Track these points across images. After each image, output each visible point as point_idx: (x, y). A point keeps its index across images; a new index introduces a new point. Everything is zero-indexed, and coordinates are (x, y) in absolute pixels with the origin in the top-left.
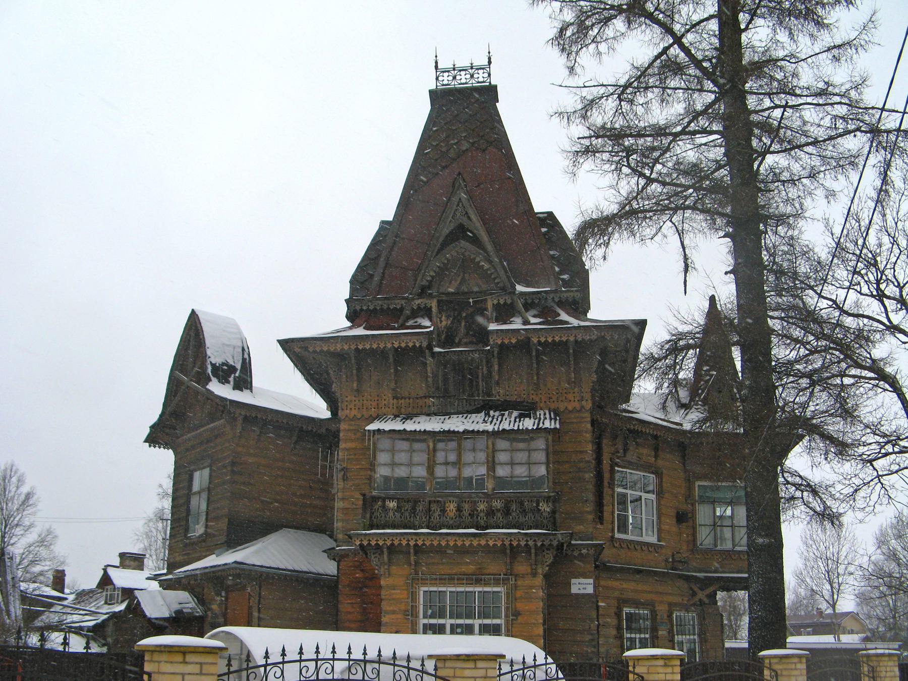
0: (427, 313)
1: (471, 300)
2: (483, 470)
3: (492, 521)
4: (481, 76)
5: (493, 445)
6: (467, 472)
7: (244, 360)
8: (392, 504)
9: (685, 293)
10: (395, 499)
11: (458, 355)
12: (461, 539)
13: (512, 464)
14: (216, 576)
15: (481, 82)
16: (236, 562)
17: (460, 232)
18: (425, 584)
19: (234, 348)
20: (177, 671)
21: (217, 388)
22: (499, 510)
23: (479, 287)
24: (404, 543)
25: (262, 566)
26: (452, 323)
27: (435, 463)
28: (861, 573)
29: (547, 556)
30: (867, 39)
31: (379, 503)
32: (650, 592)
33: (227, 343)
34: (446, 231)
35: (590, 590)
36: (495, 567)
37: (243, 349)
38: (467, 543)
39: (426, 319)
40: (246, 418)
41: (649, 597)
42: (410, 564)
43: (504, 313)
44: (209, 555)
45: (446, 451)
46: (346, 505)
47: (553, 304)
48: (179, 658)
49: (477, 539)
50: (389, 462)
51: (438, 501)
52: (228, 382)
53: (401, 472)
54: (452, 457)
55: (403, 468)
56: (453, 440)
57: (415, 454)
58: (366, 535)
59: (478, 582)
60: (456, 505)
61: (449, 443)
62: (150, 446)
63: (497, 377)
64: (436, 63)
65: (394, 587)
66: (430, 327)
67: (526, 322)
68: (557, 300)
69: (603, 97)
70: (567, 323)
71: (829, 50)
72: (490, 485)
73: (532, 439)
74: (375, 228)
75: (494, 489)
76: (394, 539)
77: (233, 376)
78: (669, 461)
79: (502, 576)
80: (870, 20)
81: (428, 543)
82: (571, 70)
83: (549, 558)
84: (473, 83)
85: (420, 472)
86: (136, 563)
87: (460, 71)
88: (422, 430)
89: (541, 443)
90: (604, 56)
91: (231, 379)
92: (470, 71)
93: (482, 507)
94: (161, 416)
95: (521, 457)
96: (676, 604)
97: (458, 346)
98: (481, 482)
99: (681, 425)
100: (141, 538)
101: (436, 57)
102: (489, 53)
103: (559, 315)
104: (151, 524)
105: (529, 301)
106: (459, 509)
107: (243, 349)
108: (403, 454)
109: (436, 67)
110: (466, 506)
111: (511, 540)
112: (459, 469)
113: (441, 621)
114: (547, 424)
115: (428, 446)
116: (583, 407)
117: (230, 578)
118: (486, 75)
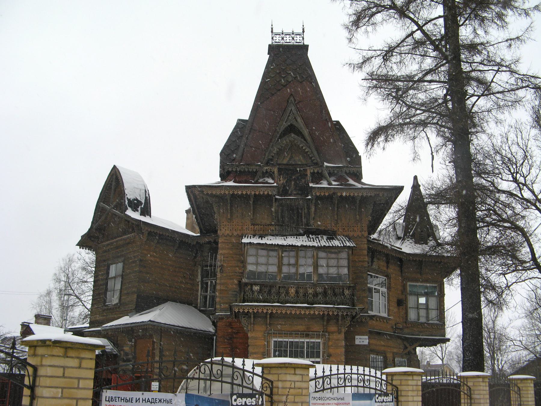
0: (271, 176)
1: (298, 169)
2: (310, 269)
3: (316, 299)
4: (298, 39)
5: (317, 254)
6: (301, 270)
7: (146, 198)
8: (256, 288)
9: (433, 171)
10: (259, 285)
11: (291, 201)
12: (299, 310)
14: (130, 330)
15: (298, 43)
16: (150, 321)
17: (292, 129)
18: (274, 337)
19: (140, 190)
20: (292, 380)
21: (130, 213)
22: (321, 293)
23: (301, 162)
24: (260, 311)
25: (165, 324)
26: (286, 182)
27: (282, 264)
29: (346, 321)
30: (528, 37)
31: (249, 287)
32: (384, 346)
33: (136, 187)
34: (282, 128)
36: (317, 327)
37: (146, 191)
38: (303, 312)
39: (270, 178)
40: (150, 233)
41: (383, 348)
42: (266, 324)
43: (318, 177)
44: (122, 317)
45: (289, 257)
46: (223, 288)
47: (344, 174)
48: (292, 371)
49: (309, 310)
50: (255, 262)
51: (284, 287)
52: (138, 211)
53: (262, 269)
54: (292, 261)
55: (263, 266)
56: (294, 251)
57: (270, 259)
58: (242, 305)
59: (307, 336)
60: (295, 290)
61: (291, 253)
62: (80, 248)
63: (313, 215)
64: (272, 29)
65: (256, 338)
66: (274, 184)
67: (330, 184)
68: (348, 172)
69: (373, 57)
70: (354, 186)
71: (507, 41)
72: (315, 278)
73: (339, 252)
74: (234, 124)
75: (317, 281)
76: (259, 309)
77: (140, 207)
78: (393, 270)
79: (321, 333)
80: (530, 26)
81: (279, 312)
82: (350, 40)
83: (348, 322)
84: (293, 42)
85: (273, 269)
86: (46, 321)
87: (286, 35)
88: (276, 244)
89: (344, 255)
90: (370, 34)
91: (139, 209)
92: (292, 35)
93: (310, 291)
94: (89, 230)
95: (333, 262)
96: (397, 354)
97: (290, 195)
98: (309, 276)
99: (401, 249)
100: (35, 306)
101: (272, 25)
102: (303, 26)
103: (348, 181)
104: (42, 298)
105: (332, 171)
106: (297, 292)
107: (146, 191)
108: (263, 258)
109: (272, 32)
110: (301, 291)
111: (328, 312)
112: (297, 268)
114: (348, 244)
115: (279, 254)
116: (363, 235)
117: (140, 331)
118: (274, 38)
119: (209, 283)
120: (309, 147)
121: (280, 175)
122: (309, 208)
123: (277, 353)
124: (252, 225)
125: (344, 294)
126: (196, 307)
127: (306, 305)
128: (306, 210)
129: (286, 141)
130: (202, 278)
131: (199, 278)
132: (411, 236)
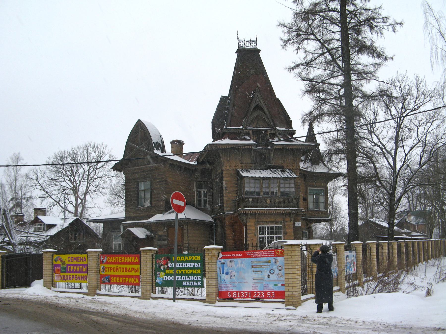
2: (277, 189)
3: (280, 205)
4: (254, 44)
6: (272, 190)
7: (162, 140)
8: (251, 200)
13: (285, 188)
24: (254, 212)
28: (57, 188)
35: (300, 225)
36: (279, 219)
55: (253, 188)
58: (245, 210)
59: (276, 223)
64: (238, 37)
81: (261, 212)
84: (250, 47)
89: (292, 181)
91: (160, 148)
93: (277, 201)
95: (287, 185)
106: (271, 201)
109: (238, 39)
110: (273, 200)
113: (273, 236)
119: (202, 192)
120: (268, 119)
121: (253, 134)
122: (269, 154)
123: (261, 233)
124: (240, 163)
125: (293, 202)
126: (194, 206)
127: (276, 208)
128: (268, 155)
129: (255, 114)
130: (197, 188)
131: (195, 189)
132: (310, 160)
